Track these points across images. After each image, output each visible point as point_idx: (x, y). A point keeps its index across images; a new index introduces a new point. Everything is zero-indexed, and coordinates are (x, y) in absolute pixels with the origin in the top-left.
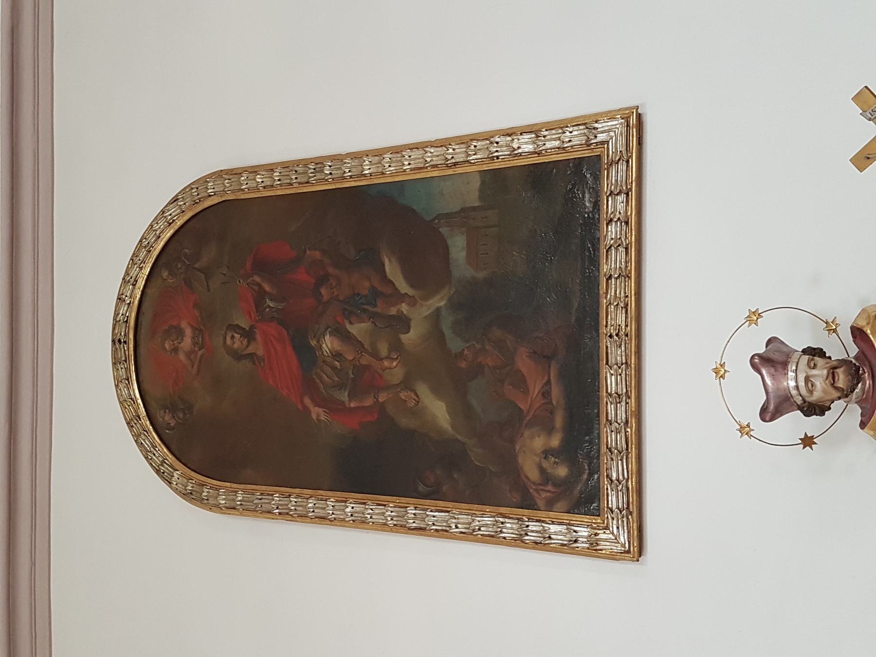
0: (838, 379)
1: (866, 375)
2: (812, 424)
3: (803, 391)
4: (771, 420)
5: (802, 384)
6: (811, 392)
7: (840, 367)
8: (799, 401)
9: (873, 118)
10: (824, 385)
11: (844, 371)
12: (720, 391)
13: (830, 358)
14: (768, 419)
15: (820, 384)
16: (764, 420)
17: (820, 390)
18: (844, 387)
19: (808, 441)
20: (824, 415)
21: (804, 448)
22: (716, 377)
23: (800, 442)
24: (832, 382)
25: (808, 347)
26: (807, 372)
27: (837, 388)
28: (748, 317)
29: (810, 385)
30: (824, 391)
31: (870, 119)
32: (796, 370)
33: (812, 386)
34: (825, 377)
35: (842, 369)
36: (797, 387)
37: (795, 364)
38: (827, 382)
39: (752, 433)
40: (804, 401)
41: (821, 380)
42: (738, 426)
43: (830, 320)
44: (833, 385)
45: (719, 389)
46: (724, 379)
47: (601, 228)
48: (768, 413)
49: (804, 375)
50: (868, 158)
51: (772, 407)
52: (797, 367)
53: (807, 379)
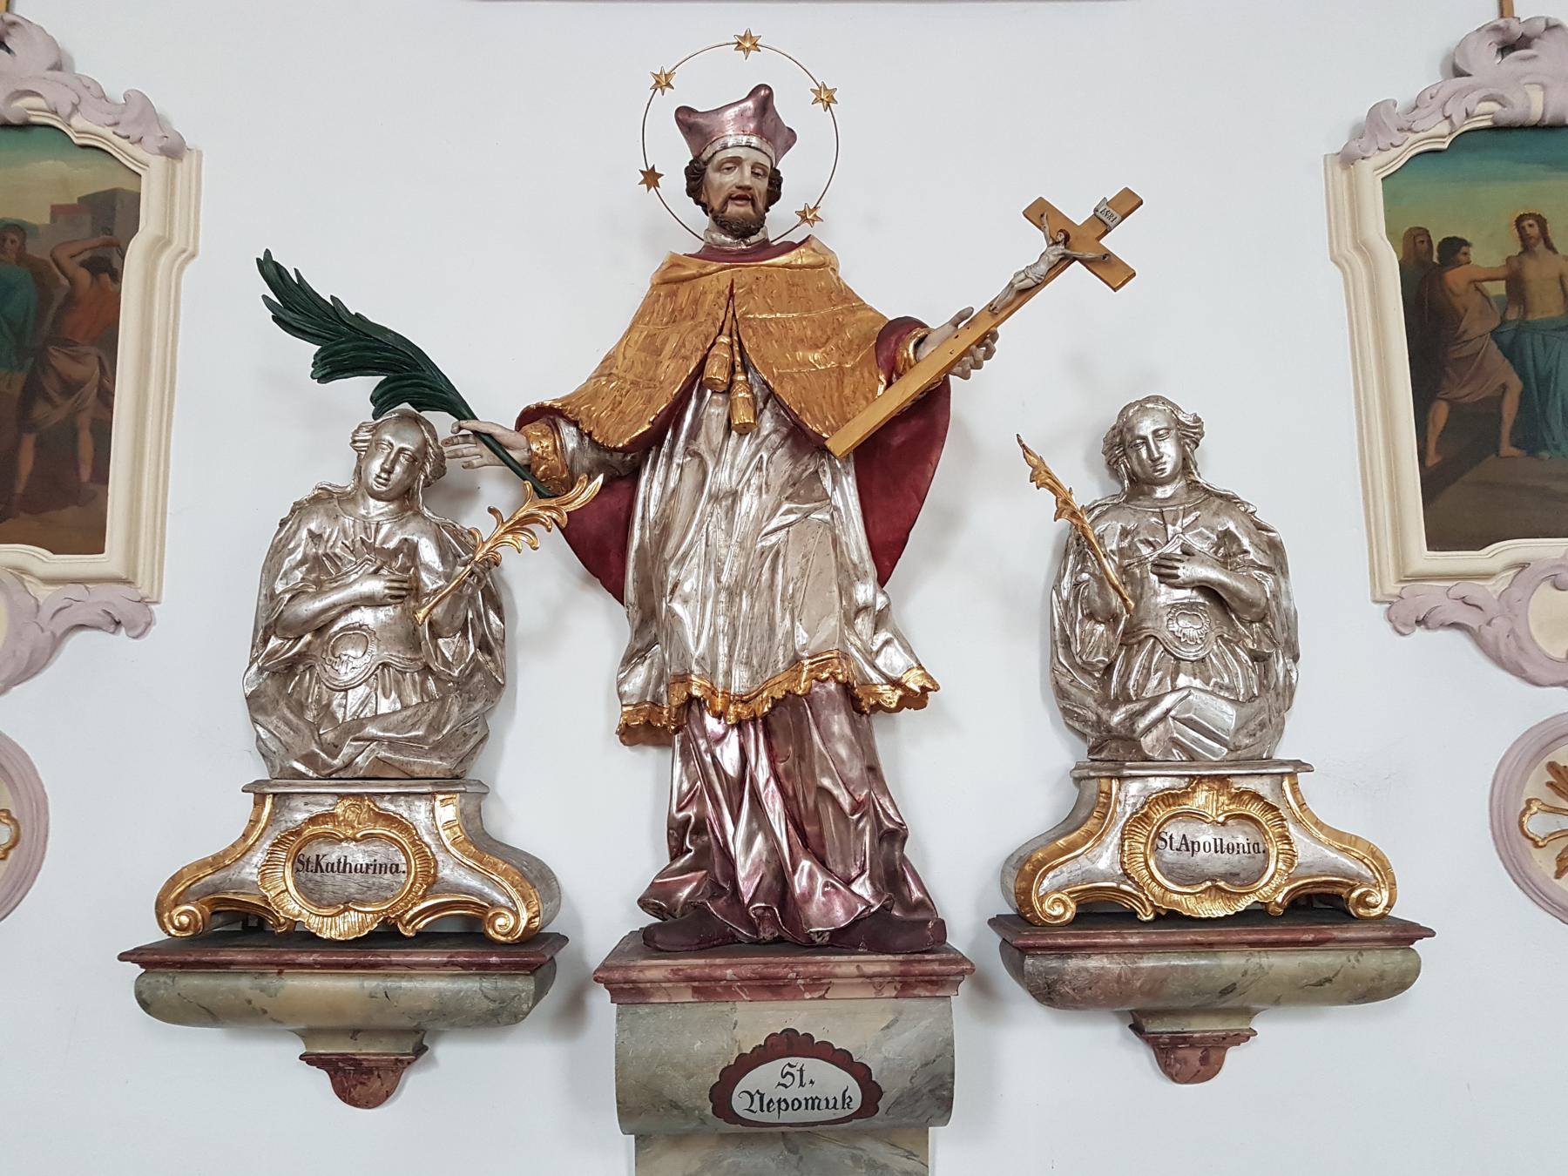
0: (738, 205)
1: (744, 247)
2: (674, 181)
3: (720, 156)
4: (678, 120)
5: (730, 153)
6: (719, 169)
7: (754, 211)
8: (705, 156)
9: (1098, 214)
10: (730, 185)
11: (747, 214)
12: (718, 43)
13: (767, 210)
14: (680, 117)
15: (730, 180)
16: (678, 110)
17: (723, 181)
18: (726, 214)
19: (651, 178)
20: (689, 195)
21: (642, 172)
22: (739, 37)
23: (650, 167)
24: (734, 196)
25: (631, 932)
26: (746, 160)
27: (725, 203)
28: (826, 89)
29: (729, 165)
30: (721, 185)
31: (1096, 210)
32: (750, 147)
33: (728, 169)
34: (741, 184)
35: (752, 212)
36: (725, 147)
37: (759, 147)
38: (734, 189)
39: (659, 90)
40: (706, 163)
41: (736, 181)
42: (670, 69)
43: (818, 213)
44: (730, 198)
45: (722, 43)
46: (736, 49)
47: (871, 408)
48: (688, 121)
49: (743, 157)
50: (1042, 216)
51: (692, 120)
52: (754, 148)
53: (737, 161)
